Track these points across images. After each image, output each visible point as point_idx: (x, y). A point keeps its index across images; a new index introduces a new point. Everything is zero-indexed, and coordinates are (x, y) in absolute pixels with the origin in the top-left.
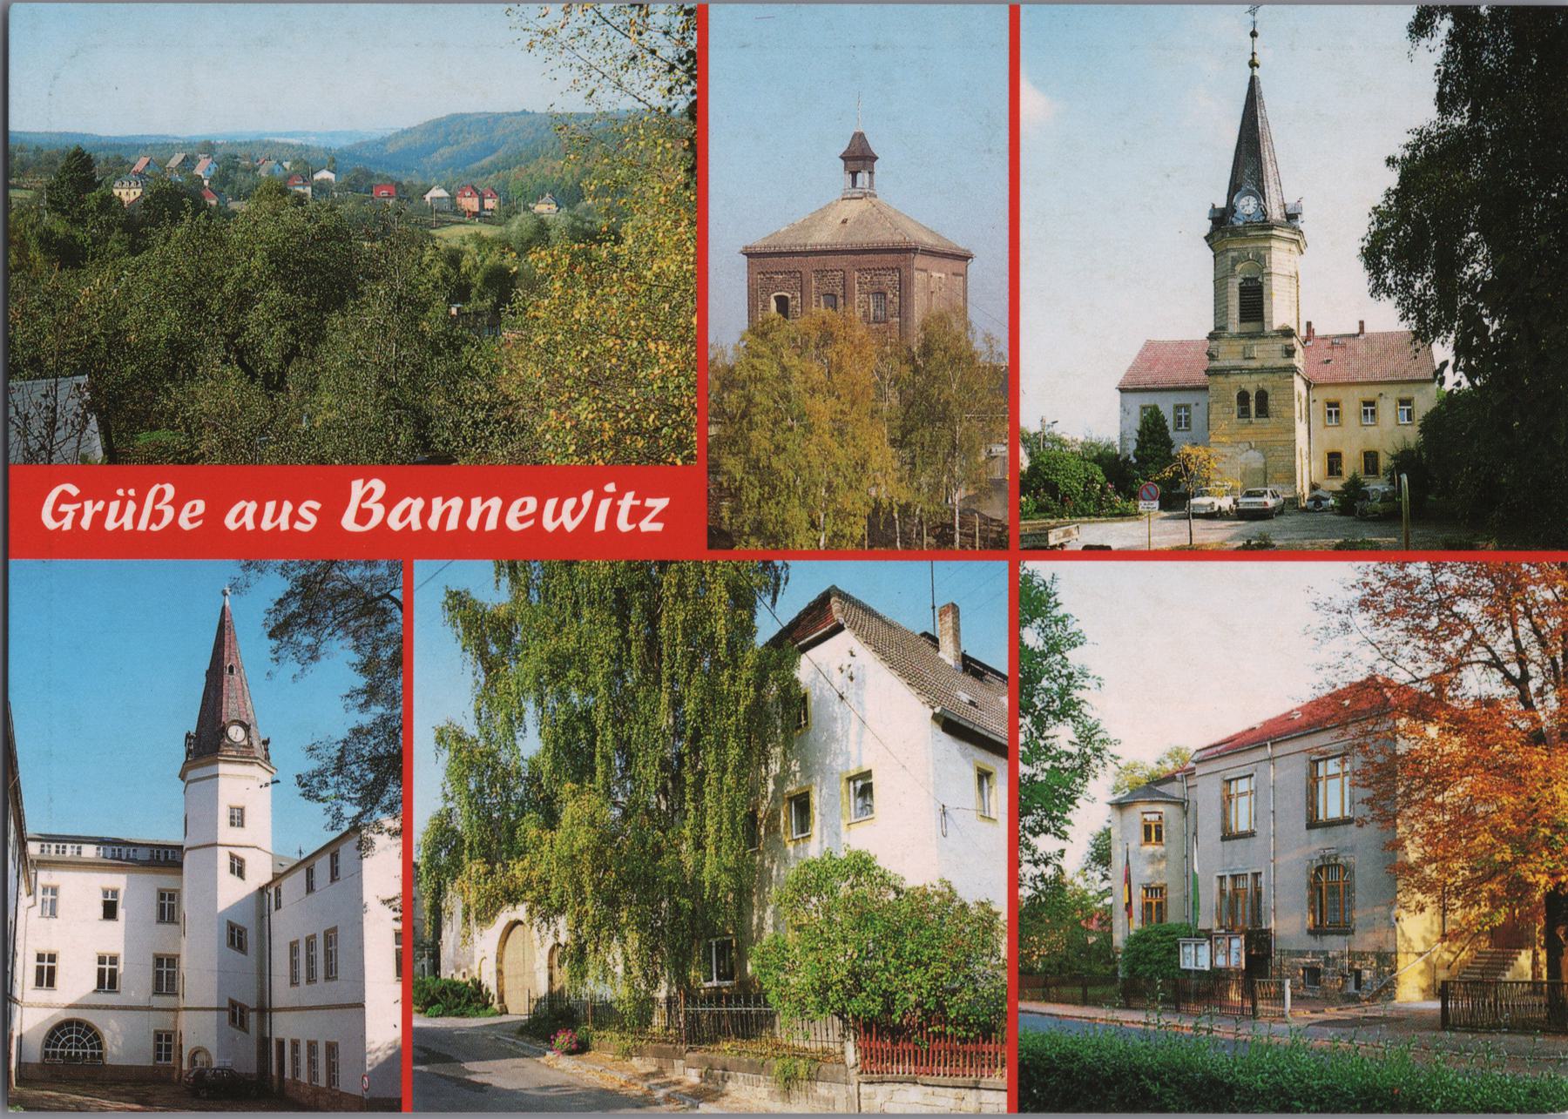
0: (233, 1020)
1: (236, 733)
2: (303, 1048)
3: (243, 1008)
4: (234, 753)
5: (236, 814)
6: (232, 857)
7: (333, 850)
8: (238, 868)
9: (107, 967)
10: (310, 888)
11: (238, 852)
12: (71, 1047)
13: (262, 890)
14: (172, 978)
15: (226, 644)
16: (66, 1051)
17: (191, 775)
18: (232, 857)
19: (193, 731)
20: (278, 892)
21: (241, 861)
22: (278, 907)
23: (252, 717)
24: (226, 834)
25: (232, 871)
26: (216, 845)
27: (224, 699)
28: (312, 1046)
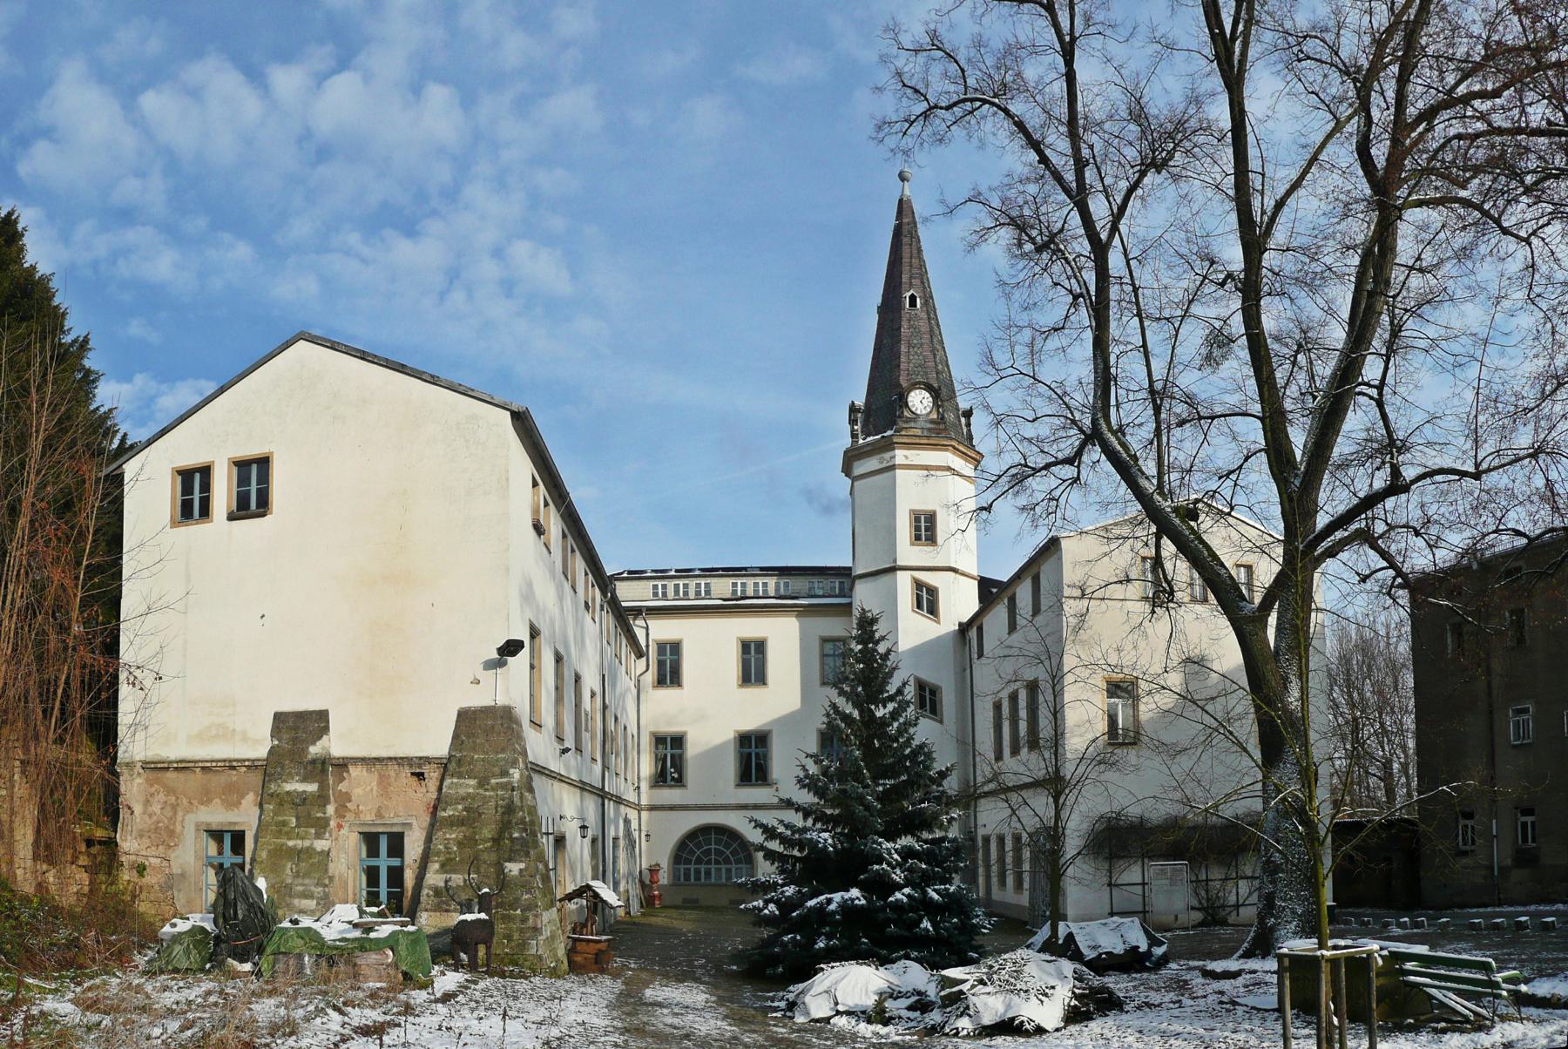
1: (919, 401)
2: (1009, 845)
4: (919, 432)
5: (668, 657)
6: (919, 585)
7: (1033, 571)
8: (927, 601)
9: (753, 750)
10: (1012, 627)
11: (926, 577)
12: (709, 862)
13: (964, 628)
14: (679, 763)
15: (905, 260)
16: (703, 868)
17: (861, 468)
18: (919, 585)
19: (860, 402)
20: (980, 629)
21: (932, 591)
22: (981, 655)
23: (609, 651)
24: (908, 552)
25: (919, 606)
26: (894, 569)
27: (903, 349)
28: (1001, 839)
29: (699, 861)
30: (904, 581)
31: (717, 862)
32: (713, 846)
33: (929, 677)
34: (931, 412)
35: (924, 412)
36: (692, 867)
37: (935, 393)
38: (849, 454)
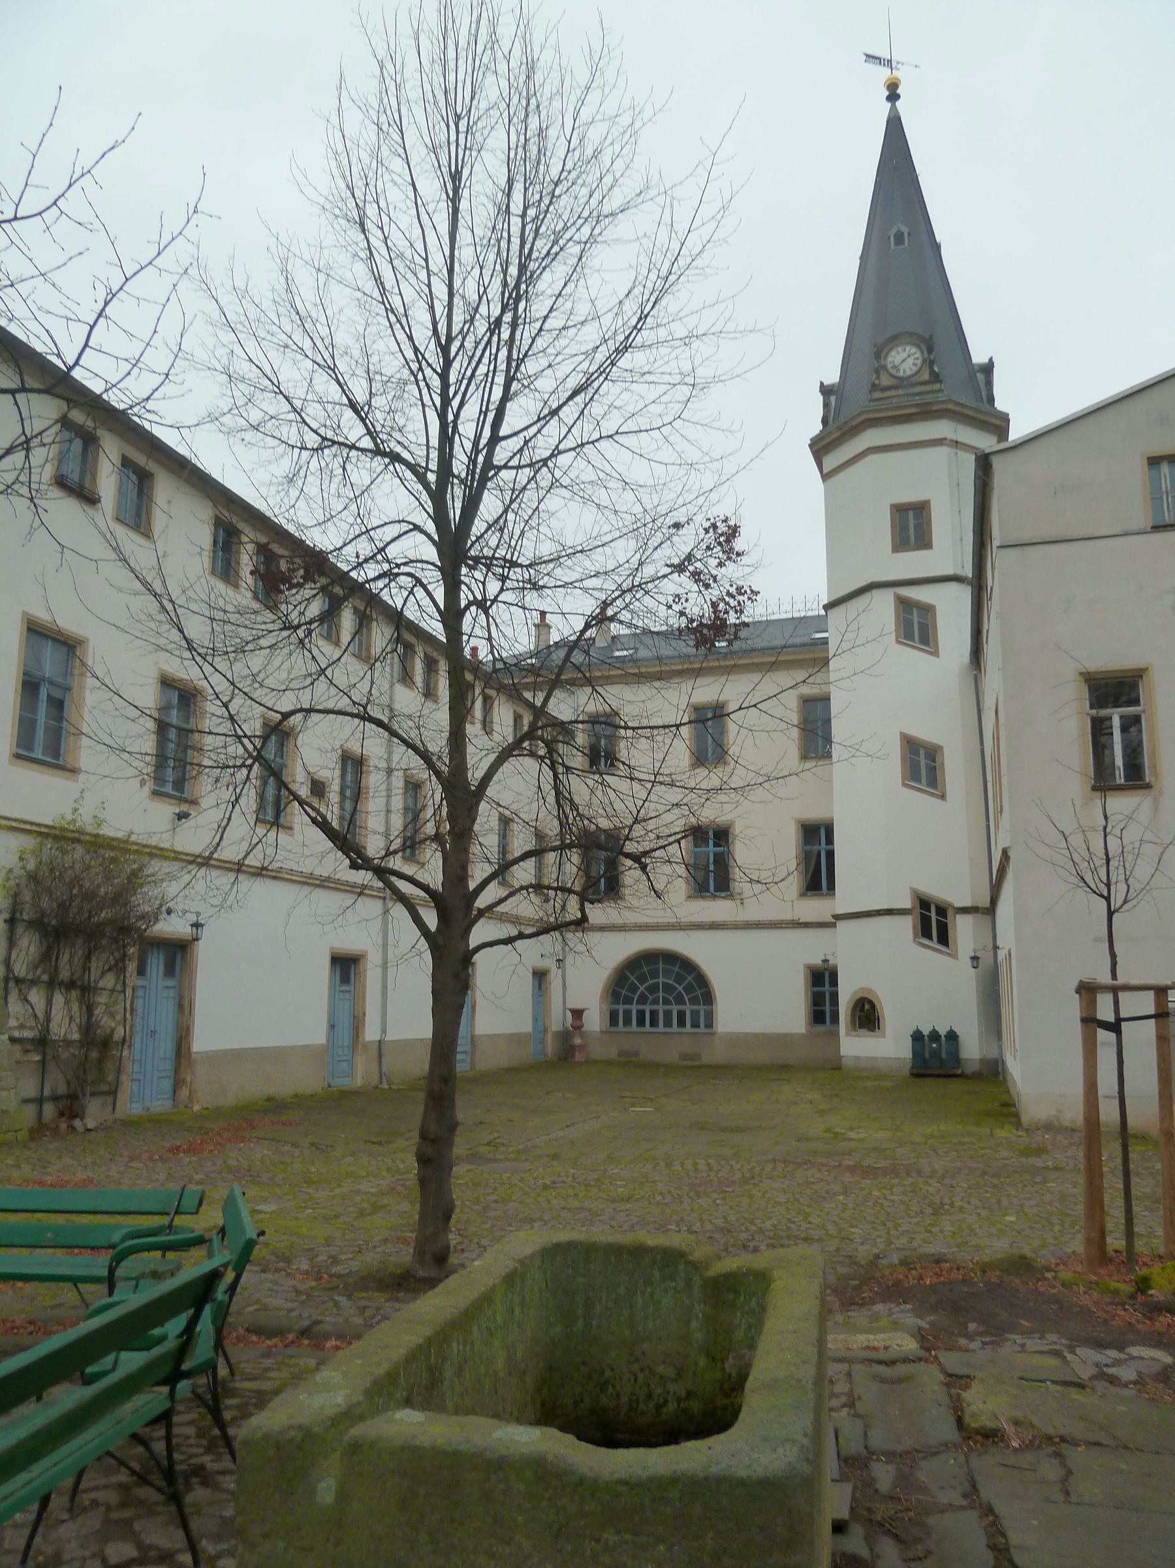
0: (925, 930)
3: (942, 911)
6: (904, 605)
12: (656, 1002)
16: (647, 1008)
29: (643, 1000)
30: (883, 605)
31: (666, 1002)
32: (661, 980)
33: (925, 733)
34: (919, 371)
35: (908, 373)
36: (634, 1008)
37: (928, 345)
38: (816, 448)
